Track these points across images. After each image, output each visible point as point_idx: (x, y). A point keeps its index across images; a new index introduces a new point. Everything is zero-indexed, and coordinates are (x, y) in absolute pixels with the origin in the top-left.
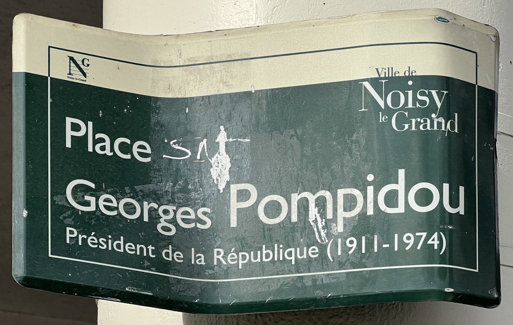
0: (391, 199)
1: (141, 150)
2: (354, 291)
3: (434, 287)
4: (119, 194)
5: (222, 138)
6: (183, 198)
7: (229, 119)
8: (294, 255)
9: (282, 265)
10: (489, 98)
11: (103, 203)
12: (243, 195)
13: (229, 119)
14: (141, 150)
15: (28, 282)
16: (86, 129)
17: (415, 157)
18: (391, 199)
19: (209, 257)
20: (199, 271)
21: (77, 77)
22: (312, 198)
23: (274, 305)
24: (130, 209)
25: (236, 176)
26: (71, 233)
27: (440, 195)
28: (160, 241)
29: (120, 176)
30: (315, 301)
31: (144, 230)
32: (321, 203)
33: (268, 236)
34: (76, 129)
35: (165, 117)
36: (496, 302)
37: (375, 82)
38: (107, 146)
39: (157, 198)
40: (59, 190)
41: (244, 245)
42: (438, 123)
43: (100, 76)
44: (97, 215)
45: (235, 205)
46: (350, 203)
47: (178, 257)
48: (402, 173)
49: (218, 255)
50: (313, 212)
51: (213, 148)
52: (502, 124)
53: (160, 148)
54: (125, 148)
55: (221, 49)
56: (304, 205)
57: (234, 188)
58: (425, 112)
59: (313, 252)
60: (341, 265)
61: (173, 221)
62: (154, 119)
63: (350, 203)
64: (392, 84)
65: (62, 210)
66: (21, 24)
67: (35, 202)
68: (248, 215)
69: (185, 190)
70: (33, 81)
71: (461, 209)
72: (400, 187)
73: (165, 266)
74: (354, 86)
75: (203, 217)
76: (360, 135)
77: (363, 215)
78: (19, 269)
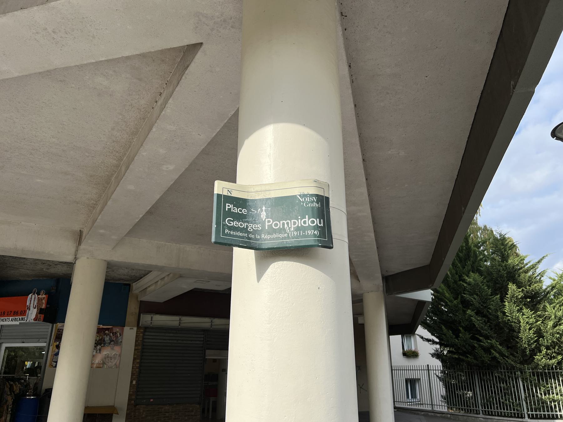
0: (305, 222)
1: (244, 211)
2: (296, 245)
3: (316, 244)
4: (239, 221)
5: (264, 208)
6: (254, 222)
7: (265, 204)
8: (281, 236)
9: (278, 238)
10: (327, 199)
11: (235, 224)
12: (269, 222)
13: (265, 204)
14: (244, 211)
15: (215, 243)
16: (231, 206)
17: (310, 212)
18: (305, 222)
19: (260, 237)
20: (258, 240)
21: (229, 194)
22: (285, 222)
23: (276, 248)
24: (241, 225)
25: (267, 217)
26: (226, 231)
27: (317, 222)
28: (249, 233)
29: (240, 217)
30: (287, 247)
31: (245, 230)
32: (288, 223)
33: (275, 231)
34: (229, 206)
35: (250, 204)
36: (332, 248)
37: (300, 195)
38: (236, 210)
39: (248, 222)
40: (224, 220)
41: (269, 233)
42: (315, 205)
43: (235, 194)
44: (233, 226)
45: (267, 224)
46: (295, 223)
47: (253, 236)
48: (307, 216)
49: (263, 236)
50: (286, 225)
51: (262, 211)
52: (331, 205)
53: (249, 210)
54: (240, 211)
55: (263, 188)
56: (283, 224)
57: (267, 220)
58: (312, 202)
59: (286, 235)
60: (293, 238)
61: (252, 228)
62: (247, 204)
63: (295, 223)
64: (304, 196)
65: (224, 225)
66: (217, 183)
67: (218, 223)
68: (230, 209)
69: (254, 220)
70: (219, 196)
71: (322, 225)
72: (307, 220)
73: (250, 239)
74: (295, 197)
75: (259, 227)
76: (297, 207)
77: (298, 226)
78: (213, 240)
